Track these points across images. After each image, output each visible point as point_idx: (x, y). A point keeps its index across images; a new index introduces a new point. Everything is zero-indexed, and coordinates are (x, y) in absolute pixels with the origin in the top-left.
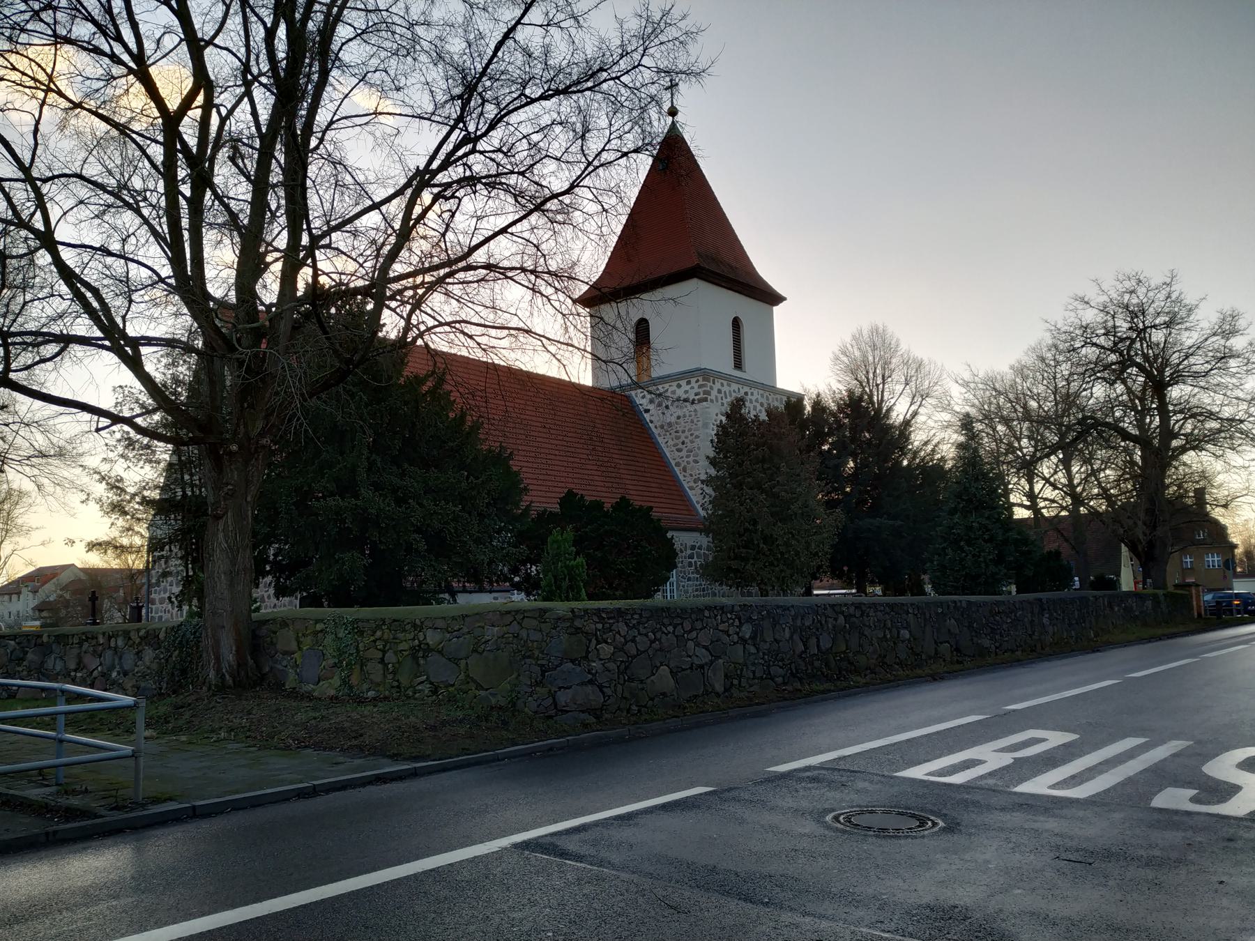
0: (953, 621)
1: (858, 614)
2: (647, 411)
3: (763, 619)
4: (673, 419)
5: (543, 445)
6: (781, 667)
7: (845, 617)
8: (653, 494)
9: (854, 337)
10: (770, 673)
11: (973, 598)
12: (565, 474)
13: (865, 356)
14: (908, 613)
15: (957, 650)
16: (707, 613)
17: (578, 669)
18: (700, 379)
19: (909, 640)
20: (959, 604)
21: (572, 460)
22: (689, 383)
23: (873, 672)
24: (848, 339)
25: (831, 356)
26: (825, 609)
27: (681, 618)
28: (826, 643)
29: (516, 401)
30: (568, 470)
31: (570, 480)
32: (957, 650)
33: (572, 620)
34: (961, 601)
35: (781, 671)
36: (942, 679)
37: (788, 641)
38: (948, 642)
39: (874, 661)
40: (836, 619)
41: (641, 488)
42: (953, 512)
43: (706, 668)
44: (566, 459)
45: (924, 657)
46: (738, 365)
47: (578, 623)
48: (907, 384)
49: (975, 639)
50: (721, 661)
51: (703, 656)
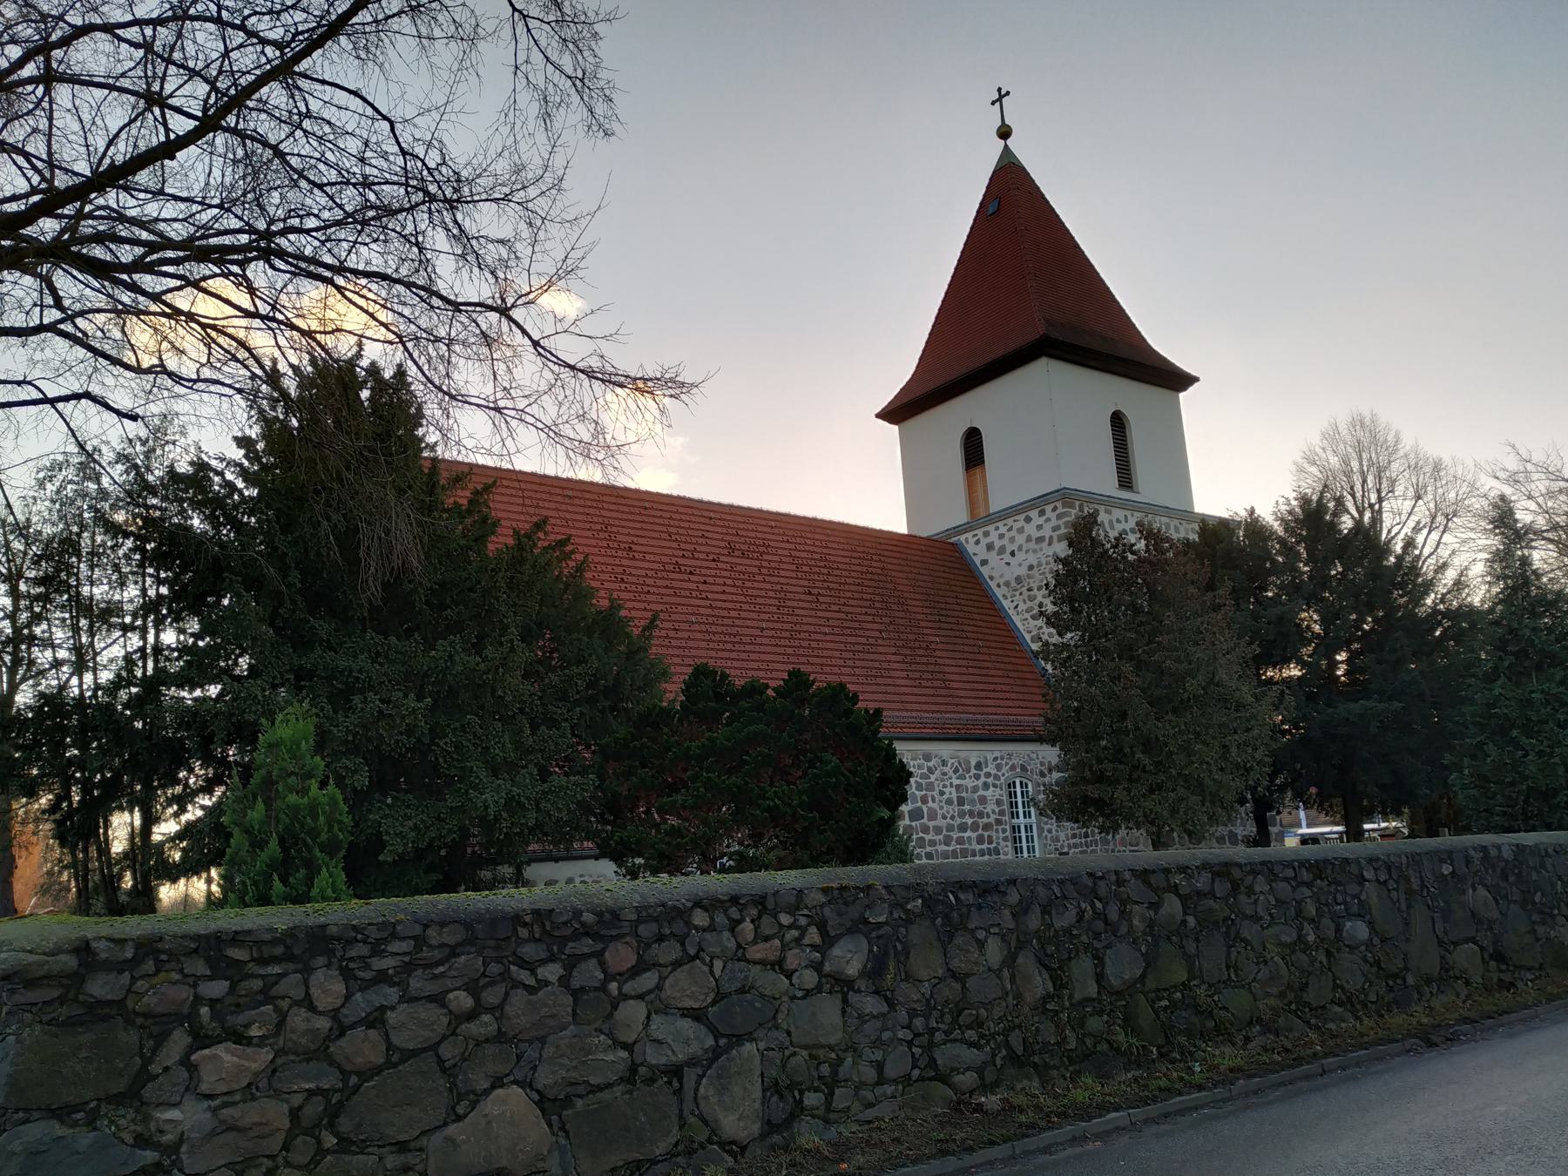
0: (1482, 891)
1: (1221, 888)
2: (984, 562)
3: (908, 921)
4: (1023, 571)
5: (805, 620)
6: (971, 1045)
7: (1184, 899)
8: (992, 687)
9: (1324, 436)
10: (932, 1063)
11: (1528, 839)
12: (841, 662)
13: (1346, 461)
14: (1362, 880)
15: (1499, 957)
16: (700, 918)
17: (85, 1139)
18: (1059, 504)
19: (1369, 944)
20: (1493, 853)
21: (853, 639)
22: (1042, 513)
23: (1267, 1029)
24: (1315, 440)
25: (1293, 468)
26: (1120, 882)
27: (595, 936)
28: (1123, 966)
29: (765, 557)
30: (846, 655)
31: (848, 671)
32: (1499, 957)
33: (76, 979)
34: (1499, 847)
35: (972, 1056)
36: (1452, 1039)
37: (998, 973)
38: (1473, 940)
39: (1272, 1001)
40: (1155, 906)
41: (972, 678)
42: (1491, 678)
43: (690, 1075)
44: (842, 639)
45: (1410, 980)
46: (1126, 478)
47: (100, 987)
48: (1418, 498)
49: (1541, 930)
50: (749, 1048)
51: (687, 1039)
